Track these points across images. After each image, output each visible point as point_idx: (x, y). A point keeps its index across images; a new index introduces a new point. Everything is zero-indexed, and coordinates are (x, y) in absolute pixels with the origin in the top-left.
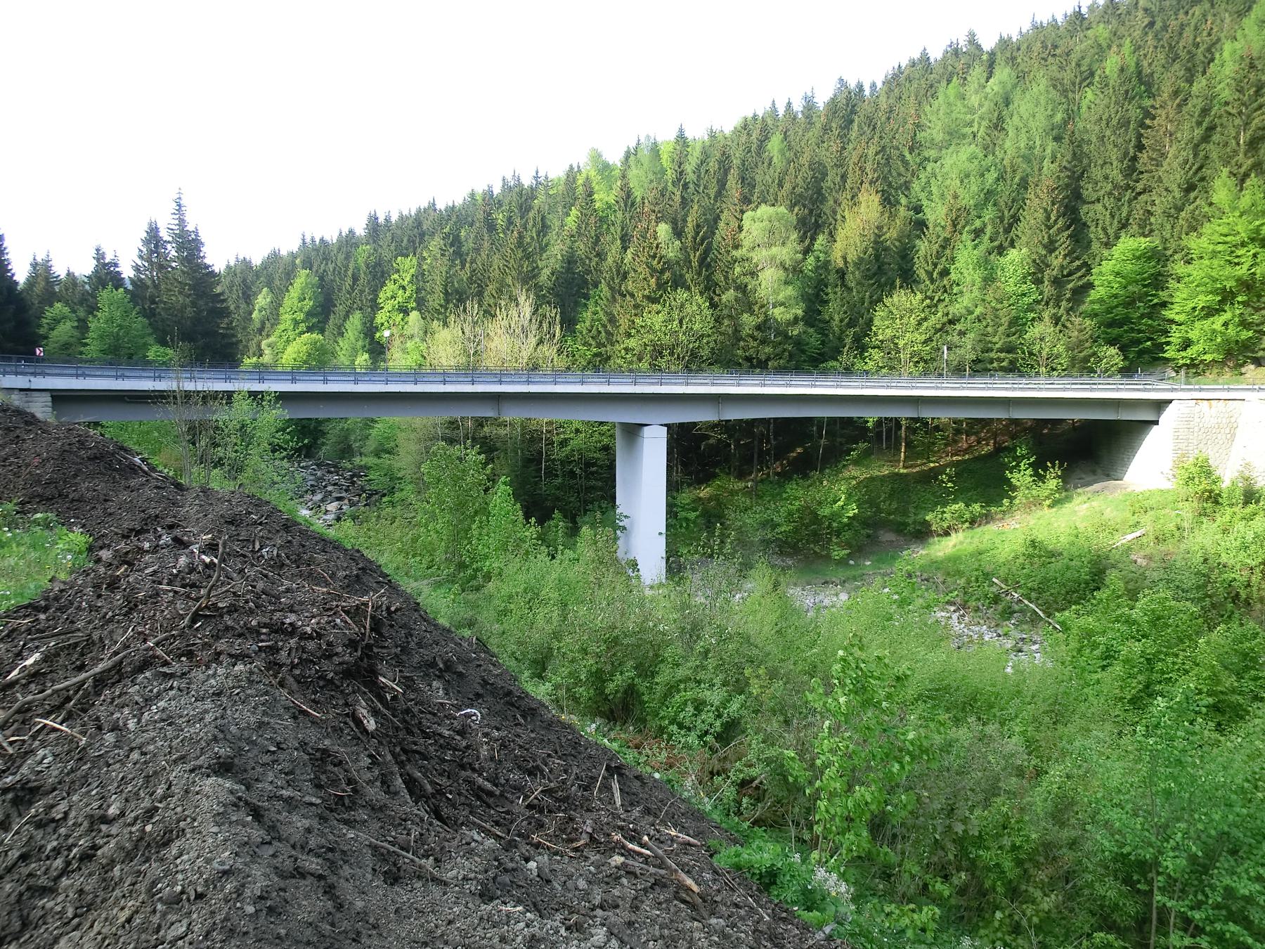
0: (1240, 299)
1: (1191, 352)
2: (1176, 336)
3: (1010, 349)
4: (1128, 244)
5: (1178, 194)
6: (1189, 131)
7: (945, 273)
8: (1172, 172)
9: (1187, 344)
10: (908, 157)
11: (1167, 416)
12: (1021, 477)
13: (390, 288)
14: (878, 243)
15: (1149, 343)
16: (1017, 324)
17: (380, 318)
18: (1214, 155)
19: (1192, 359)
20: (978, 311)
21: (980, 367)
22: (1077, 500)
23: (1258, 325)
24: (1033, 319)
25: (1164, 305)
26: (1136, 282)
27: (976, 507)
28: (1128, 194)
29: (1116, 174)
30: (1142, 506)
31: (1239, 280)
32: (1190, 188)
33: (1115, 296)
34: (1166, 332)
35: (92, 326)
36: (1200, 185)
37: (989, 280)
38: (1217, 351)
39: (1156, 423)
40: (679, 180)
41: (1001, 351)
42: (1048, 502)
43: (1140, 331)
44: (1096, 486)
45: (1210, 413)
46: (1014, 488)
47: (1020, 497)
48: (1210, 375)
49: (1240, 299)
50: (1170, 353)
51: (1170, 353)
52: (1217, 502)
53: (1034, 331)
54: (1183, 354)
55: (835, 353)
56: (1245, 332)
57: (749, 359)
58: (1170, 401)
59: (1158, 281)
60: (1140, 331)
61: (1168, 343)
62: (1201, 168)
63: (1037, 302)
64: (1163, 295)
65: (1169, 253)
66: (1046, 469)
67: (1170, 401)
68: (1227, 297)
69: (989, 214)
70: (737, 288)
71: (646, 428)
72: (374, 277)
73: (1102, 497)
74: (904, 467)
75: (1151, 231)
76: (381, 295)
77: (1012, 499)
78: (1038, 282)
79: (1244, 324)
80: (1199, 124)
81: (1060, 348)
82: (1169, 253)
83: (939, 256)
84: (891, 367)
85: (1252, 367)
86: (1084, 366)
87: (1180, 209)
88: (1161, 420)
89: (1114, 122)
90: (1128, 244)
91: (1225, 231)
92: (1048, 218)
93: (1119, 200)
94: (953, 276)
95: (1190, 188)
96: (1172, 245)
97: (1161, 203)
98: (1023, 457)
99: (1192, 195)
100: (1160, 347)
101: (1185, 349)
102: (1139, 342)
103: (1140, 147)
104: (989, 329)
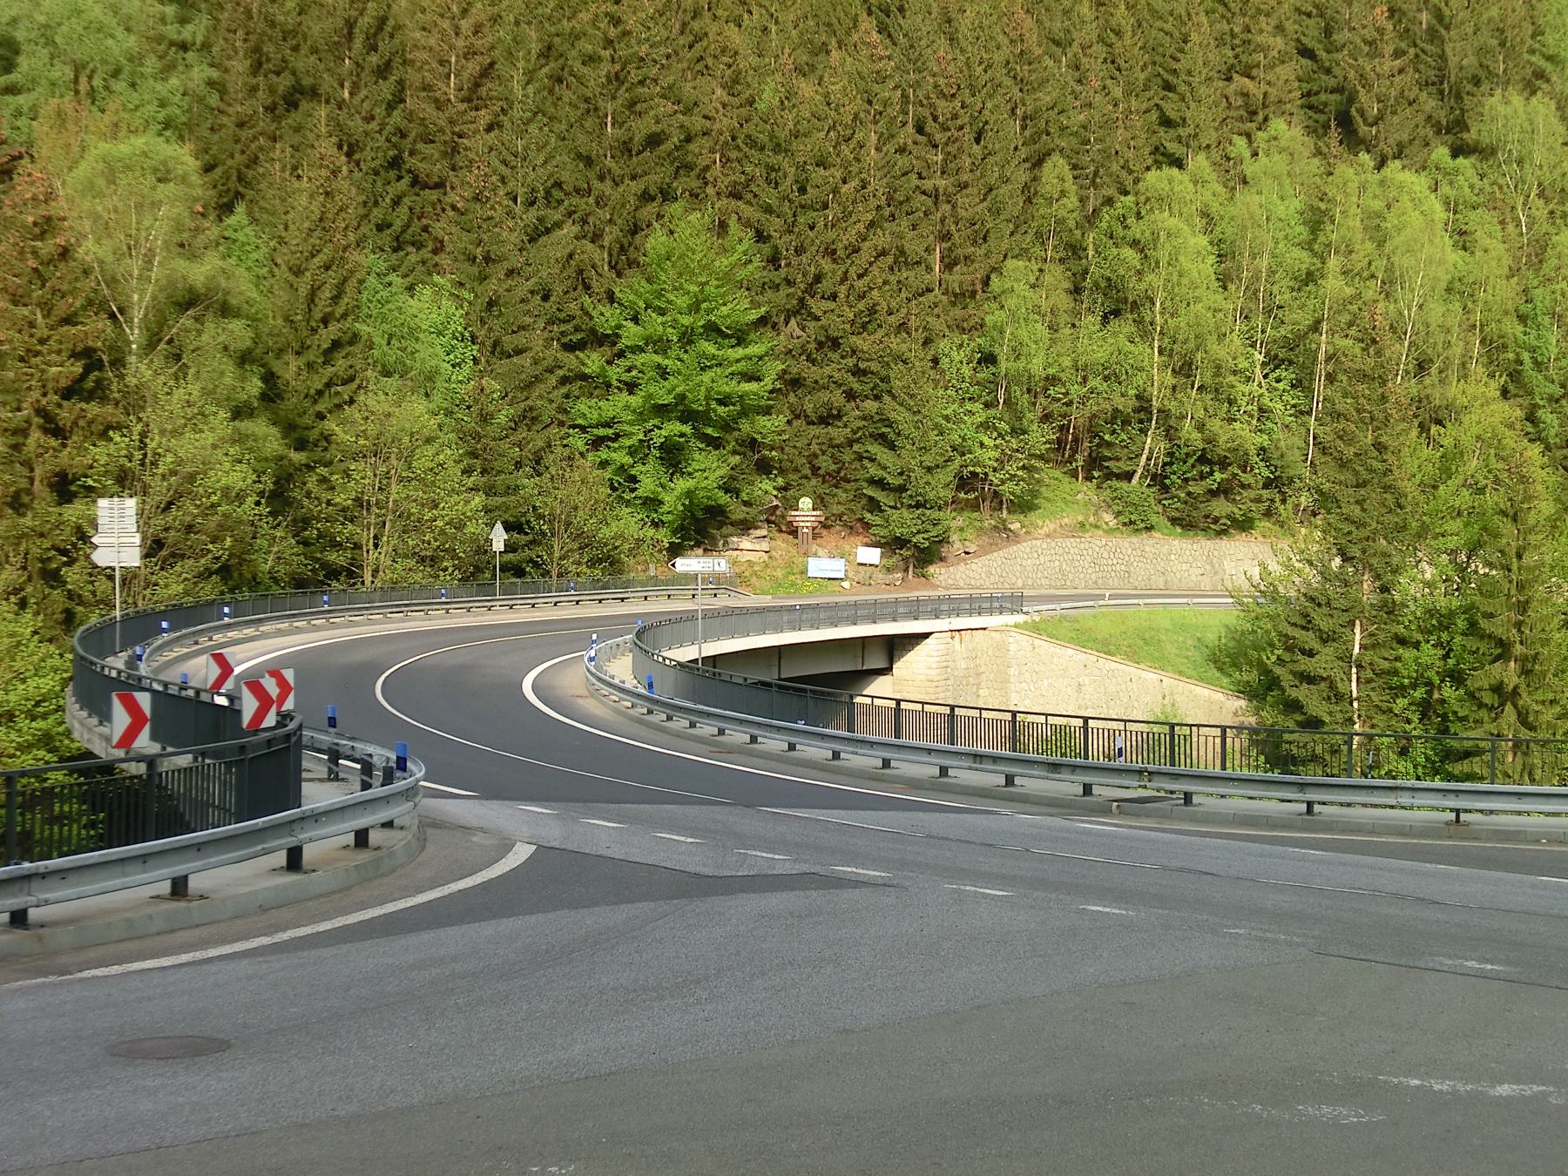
39: (887, 671)
67: (926, 636)
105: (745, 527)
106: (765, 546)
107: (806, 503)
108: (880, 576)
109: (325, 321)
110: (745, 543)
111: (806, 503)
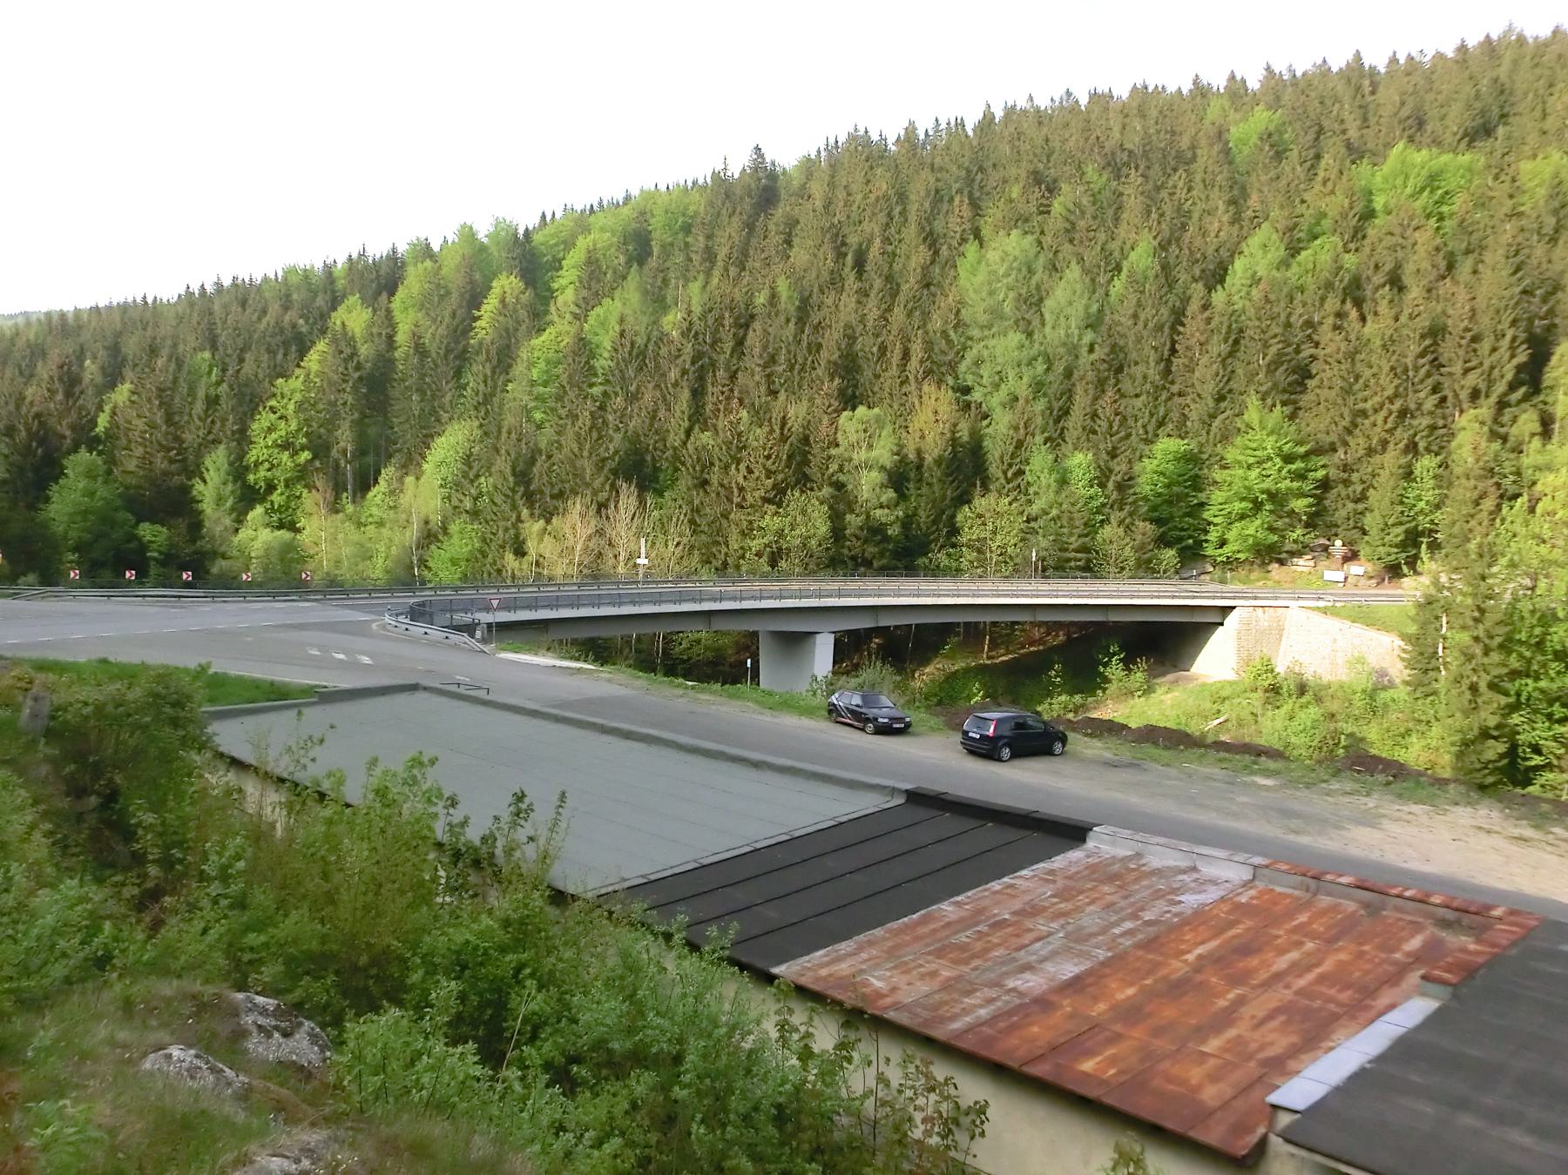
0: (1267, 507)
1: (1227, 550)
2: (1213, 536)
3: (1084, 549)
4: (1168, 446)
5: (1211, 403)
6: (1218, 347)
7: (1021, 472)
8: (1205, 376)
9: (1222, 543)
10: (952, 333)
11: (1231, 620)
12: (1115, 670)
13: (264, 419)
14: (954, 441)
15: (1191, 541)
16: (1091, 528)
17: (253, 455)
18: (1240, 371)
19: (1228, 558)
20: (1054, 512)
21: (1055, 567)
22: (1160, 691)
23: (1282, 530)
24: (1102, 521)
25: (1202, 505)
26: (1179, 484)
27: (1078, 698)
28: (1164, 395)
29: (1154, 373)
30: (1220, 697)
31: (1267, 492)
32: (1220, 398)
33: (1160, 495)
34: (1206, 532)
35: (1349, 730)
36: (1229, 396)
37: (1063, 482)
38: (1248, 551)
39: (1222, 624)
40: (689, 330)
41: (1077, 551)
42: (1139, 693)
43: (1182, 529)
44: (1170, 677)
45: (1264, 618)
46: (1107, 680)
47: (1112, 688)
48: (1242, 573)
49: (1267, 507)
50: (1210, 551)
51: (1210, 551)
52: (1278, 693)
53: (1107, 532)
54: (1220, 551)
55: (924, 550)
56: (1271, 536)
57: (854, 558)
58: (1234, 607)
59: (1197, 483)
60: (1182, 529)
61: (1207, 541)
62: (1229, 380)
63: (1103, 505)
64: (1202, 496)
65: (1205, 456)
66: (1135, 663)
67: (1234, 607)
68: (1258, 506)
69: (1040, 405)
70: (831, 484)
71: (818, 636)
72: (241, 403)
73: (1181, 688)
74: (989, 658)
75: (1187, 433)
76: (255, 426)
77: (1104, 690)
78: (1102, 485)
79: (1271, 529)
80: (1226, 341)
81: (1128, 551)
82: (1205, 456)
83: (1013, 456)
84: (982, 568)
85: (1277, 565)
86: (1146, 568)
87: (1213, 416)
88: (1226, 622)
89: (1151, 325)
90: (1168, 446)
91: (1254, 445)
92: (1111, 427)
93: (1156, 399)
94: (1029, 477)
95: (1220, 398)
96: (1208, 450)
97: (1196, 412)
98: (1114, 654)
99: (1223, 405)
100: (1199, 544)
101: (1221, 547)
102: (1180, 540)
103: (1173, 351)
104: (1065, 530)
105: (1299, 554)
106: (1312, 563)
107: (1338, 543)
108: (1363, 581)
109: (1010, 465)
110: (1301, 562)
111: (1338, 543)
